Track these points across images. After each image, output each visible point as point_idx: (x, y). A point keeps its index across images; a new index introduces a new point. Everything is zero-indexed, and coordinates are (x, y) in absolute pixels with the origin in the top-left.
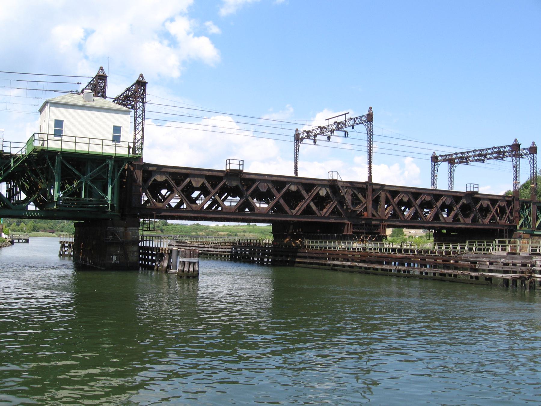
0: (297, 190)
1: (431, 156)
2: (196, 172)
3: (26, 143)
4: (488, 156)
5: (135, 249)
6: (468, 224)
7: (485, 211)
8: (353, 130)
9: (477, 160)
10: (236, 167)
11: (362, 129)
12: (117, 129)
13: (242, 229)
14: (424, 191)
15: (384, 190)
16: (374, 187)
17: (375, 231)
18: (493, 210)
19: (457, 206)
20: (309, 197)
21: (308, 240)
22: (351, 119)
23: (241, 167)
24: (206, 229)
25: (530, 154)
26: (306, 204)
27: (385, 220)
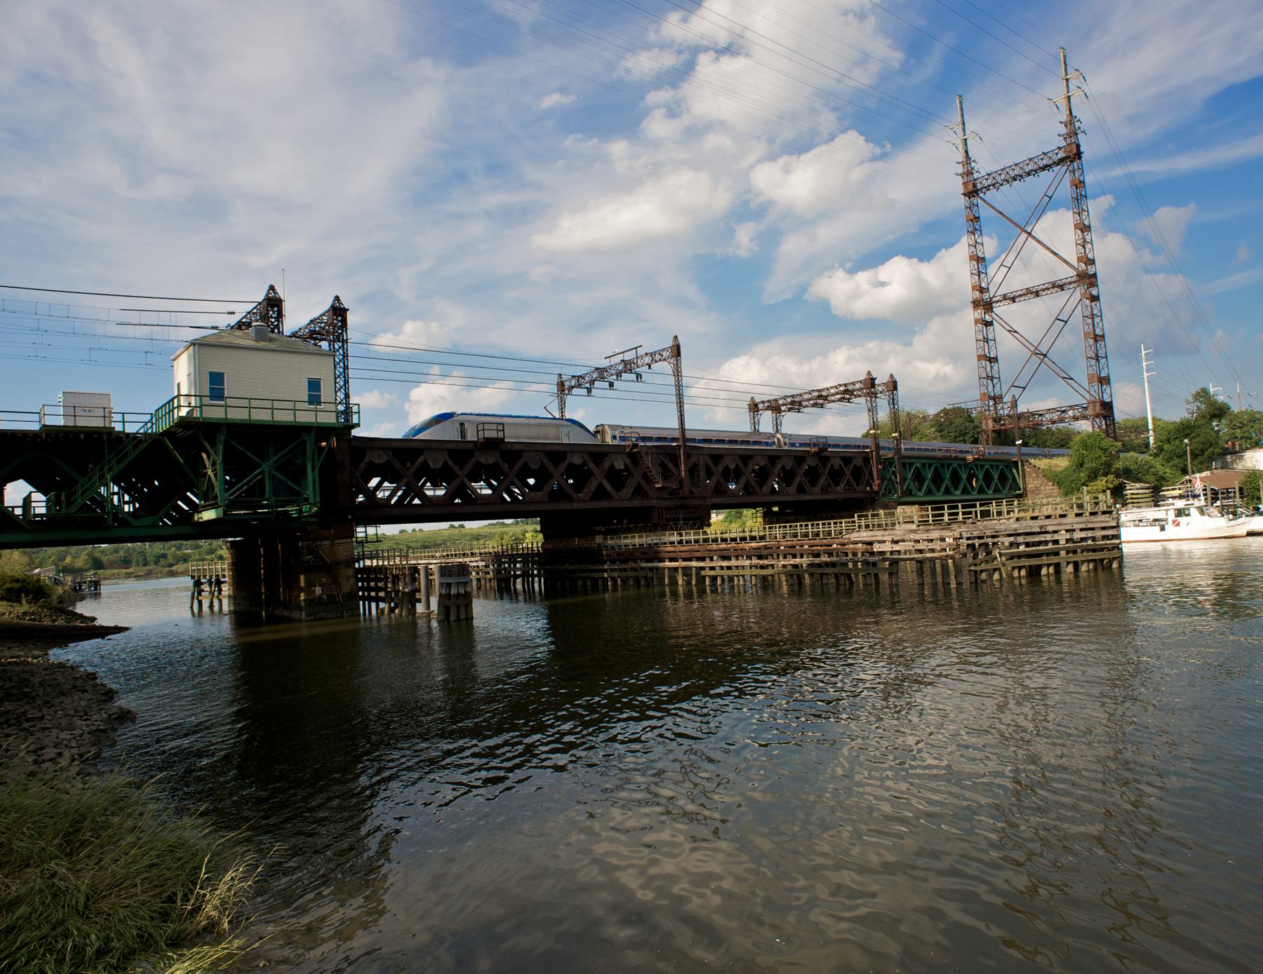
3: (152, 414)
4: (804, 404)
5: (350, 572)
7: (836, 475)
8: (650, 371)
9: (815, 405)
10: (493, 434)
11: (666, 367)
12: (314, 385)
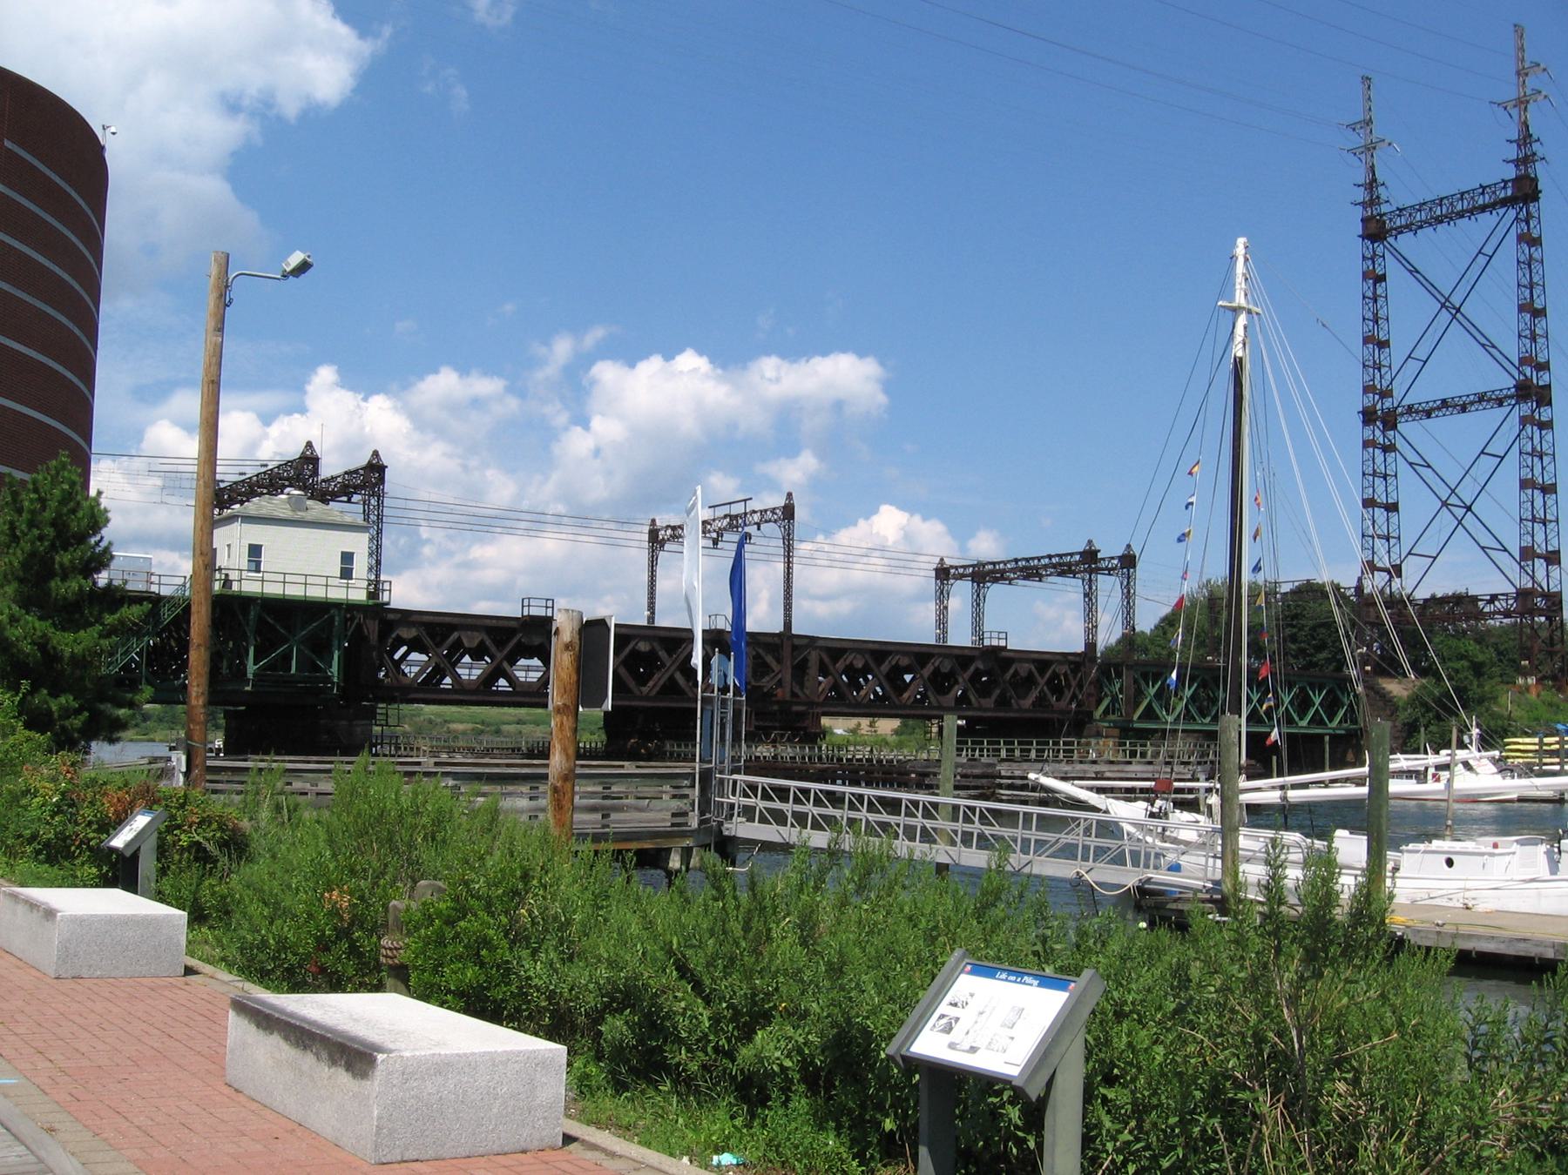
0: (650, 651)
1: (935, 566)
2: (469, 621)
3: (185, 577)
6: (986, 710)
12: (347, 558)
13: (515, 715)
14: (898, 648)
15: (816, 648)
16: (796, 642)
17: (799, 725)
18: (1042, 681)
19: (965, 676)
20: (673, 662)
21: (672, 742)
22: (754, 512)
23: (550, 610)
24: (414, 715)
25: (1122, 568)
26: (667, 676)
27: (818, 704)
